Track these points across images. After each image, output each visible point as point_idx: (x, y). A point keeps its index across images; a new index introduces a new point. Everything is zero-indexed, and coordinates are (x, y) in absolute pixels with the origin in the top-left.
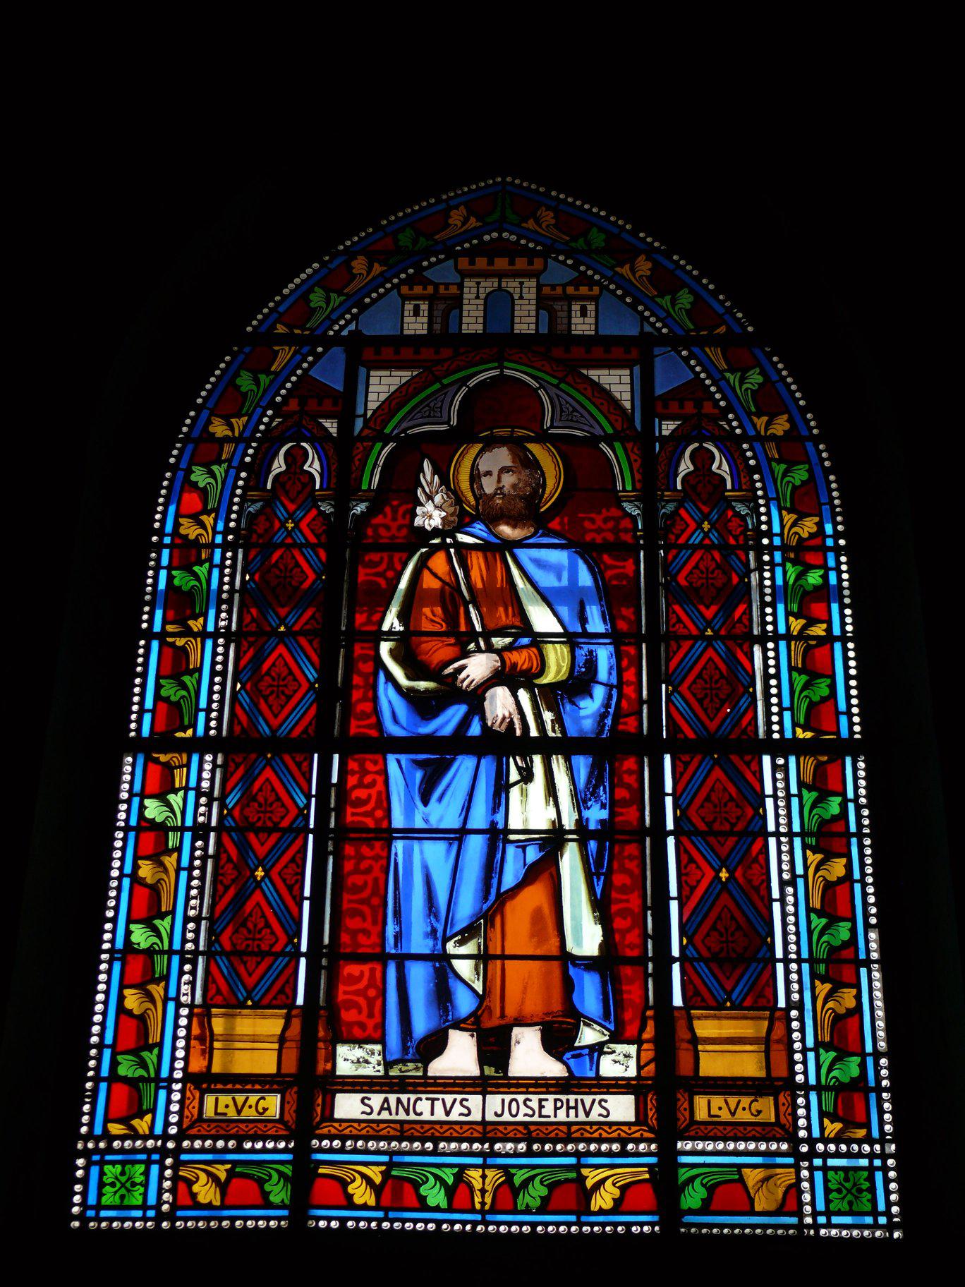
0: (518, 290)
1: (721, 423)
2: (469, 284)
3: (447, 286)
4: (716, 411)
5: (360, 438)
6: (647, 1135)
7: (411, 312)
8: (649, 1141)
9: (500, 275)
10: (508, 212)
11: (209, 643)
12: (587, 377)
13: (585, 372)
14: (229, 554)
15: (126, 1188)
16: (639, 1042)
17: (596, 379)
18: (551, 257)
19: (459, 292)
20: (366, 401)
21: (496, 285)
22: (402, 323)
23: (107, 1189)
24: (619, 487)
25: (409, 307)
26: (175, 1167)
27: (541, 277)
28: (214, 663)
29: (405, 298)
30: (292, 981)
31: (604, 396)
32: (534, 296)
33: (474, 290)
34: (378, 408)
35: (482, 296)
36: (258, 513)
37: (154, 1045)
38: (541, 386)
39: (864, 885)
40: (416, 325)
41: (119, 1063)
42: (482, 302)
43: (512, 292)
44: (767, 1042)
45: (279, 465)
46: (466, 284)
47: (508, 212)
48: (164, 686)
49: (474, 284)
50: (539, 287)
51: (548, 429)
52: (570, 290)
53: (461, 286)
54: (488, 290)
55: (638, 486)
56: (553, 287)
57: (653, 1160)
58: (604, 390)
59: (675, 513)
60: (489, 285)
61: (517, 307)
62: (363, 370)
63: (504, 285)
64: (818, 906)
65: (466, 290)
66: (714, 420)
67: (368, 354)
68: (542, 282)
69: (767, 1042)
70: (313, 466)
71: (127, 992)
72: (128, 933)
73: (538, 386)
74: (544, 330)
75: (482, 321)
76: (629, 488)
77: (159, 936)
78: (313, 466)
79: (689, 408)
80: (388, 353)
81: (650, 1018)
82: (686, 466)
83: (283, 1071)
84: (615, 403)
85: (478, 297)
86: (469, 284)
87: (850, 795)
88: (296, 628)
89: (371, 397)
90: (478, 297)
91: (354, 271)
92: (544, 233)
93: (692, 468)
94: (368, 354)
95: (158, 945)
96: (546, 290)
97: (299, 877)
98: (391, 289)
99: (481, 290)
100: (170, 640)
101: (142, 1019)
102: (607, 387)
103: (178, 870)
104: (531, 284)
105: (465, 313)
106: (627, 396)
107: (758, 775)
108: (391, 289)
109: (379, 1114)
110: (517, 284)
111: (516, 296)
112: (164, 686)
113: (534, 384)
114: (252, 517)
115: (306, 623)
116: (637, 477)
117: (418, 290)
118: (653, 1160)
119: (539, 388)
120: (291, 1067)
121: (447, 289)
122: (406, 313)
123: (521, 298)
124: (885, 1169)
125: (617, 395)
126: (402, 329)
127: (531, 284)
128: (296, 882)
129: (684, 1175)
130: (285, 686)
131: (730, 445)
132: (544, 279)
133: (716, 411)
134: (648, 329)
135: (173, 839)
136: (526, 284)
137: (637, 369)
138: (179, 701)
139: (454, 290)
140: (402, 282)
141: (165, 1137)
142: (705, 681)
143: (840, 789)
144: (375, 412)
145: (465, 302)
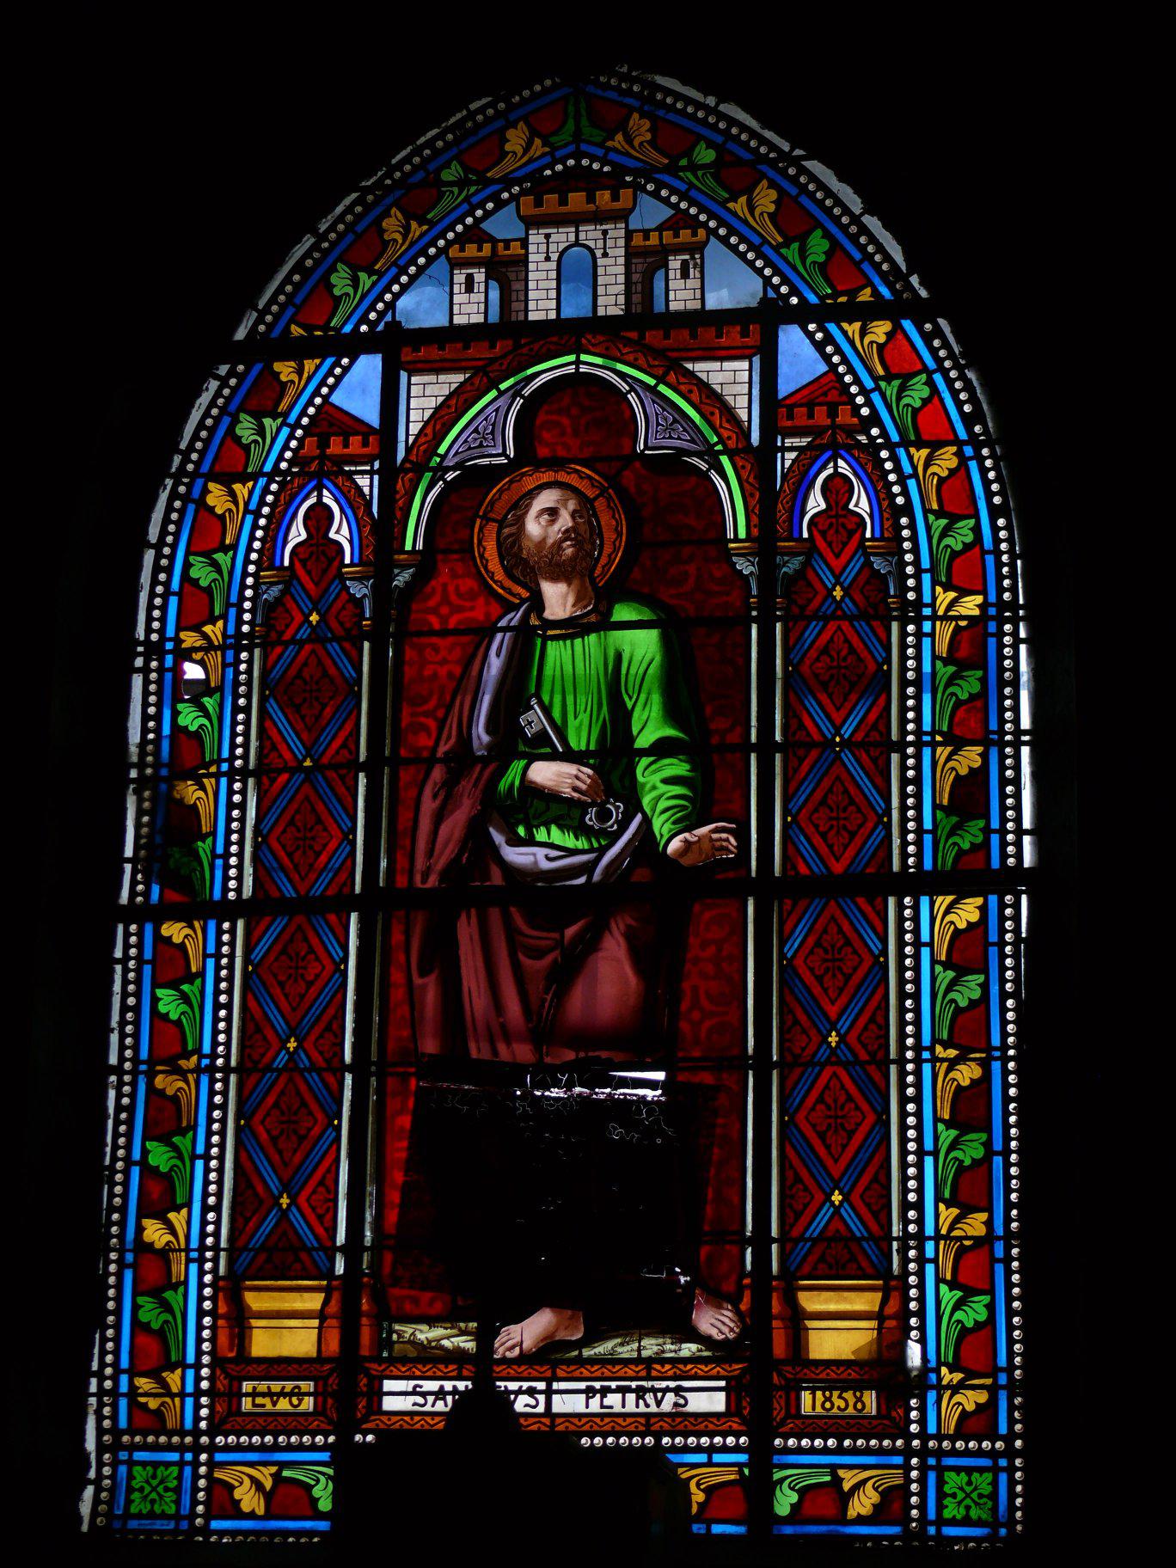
0: (600, 244)
1: (859, 438)
2: (536, 238)
3: (507, 243)
4: (855, 420)
5: (402, 469)
6: (735, 1427)
7: (463, 286)
8: (737, 1435)
9: (576, 220)
10: (587, 131)
11: (205, 1080)
12: (692, 374)
13: (689, 366)
14: (226, 925)
15: (158, 1494)
16: (735, 1301)
17: (703, 376)
18: (644, 190)
19: (523, 251)
20: (408, 422)
21: (572, 237)
22: (451, 304)
23: (136, 1496)
24: (731, 535)
25: (460, 277)
26: (211, 1464)
27: (632, 218)
28: (205, 1195)
29: (455, 264)
30: (333, 1168)
31: (710, 400)
32: (622, 252)
33: (543, 248)
34: (421, 430)
35: (554, 257)
36: (278, 600)
37: (179, 1284)
38: (632, 389)
39: (917, 563)
40: (470, 310)
41: (180, 713)
42: (553, 265)
43: (593, 247)
44: (879, 1316)
45: (298, 533)
46: (532, 239)
47: (587, 131)
48: (161, 999)
49: (542, 239)
50: (629, 235)
51: (643, 451)
52: (668, 236)
53: (525, 243)
54: (562, 247)
55: (755, 532)
56: (646, 233)
57: (743, 1458)
58: (714, 392)
59: (800, 574)
60: (562, 237)
61: (600, 271)
62: (404, 375)
63: (582, 236)
64: (947, 1117)
65: (532, 248)
66: (850, 432)
67: (407, 355)
68: (631, 227)
69: (879, 1316)
70: (341, 532)
71: (146, 1222)
72: (140, 1229)
73: (627, 388)
74: (637, 309)
75: (555, 277)
76: (742, 534)
77: (174, 1233)
78: (341, 532)
79: (821, 417)
80: (433, 353)
81: (747, 1286)
82: (816, 503)
83: (324, 1354)
84: (728, 412)
85: (548, 259)
86: (536, 238)
87: (930, 363)
88: (325, 760)
89: (414, 416)
90: (548, 259)
91: (386, 237)
92: (638, 155)
93: (823, 506)
94: (407, 355)
95: (184, 1090)
96: (637, 240)
97: (331, 1204)
98: (436, 257)
99: (553, 248)
100: (142, 1400)
101: (161, 1334)
102: (718, 388)
103: (214, 856)
104: (617, 232)
105: (532, 285)
106: (742, 402)
107: (882, 914)
108: (436, 257)
109: (433, 1406)
110: (599, 235)
111: (599, 253)
112: (161, 999)
113: (625, 387)
114: (271, 607)
115: (337, 753)
116: (755, 520)
117: (471, 250)
118: (743, 1458)
119: (629, 392)
120: (333, 1345)
121: (507, 248)
122: (456, 289)
123: (605, 255)
124: (1011, 1469)
125: (730, 400)
126: (451, 314)
127: (617, 232)
128: (328, 1210)
129: (777, 1476)
130: (313, 838)
131: (868, 461)
132: (635, 222)
133: (855, 420)
134: (771, 294)
135: (178, 1269)
136: (611, 234)
137: (756, 360)
138: (183, 942)
139: (516, 249)
140: (449, 244)
141: (200, 1433)
142: (841, 972)
143: (919, 366)
144: (418, 436)
145: (532, 266)
